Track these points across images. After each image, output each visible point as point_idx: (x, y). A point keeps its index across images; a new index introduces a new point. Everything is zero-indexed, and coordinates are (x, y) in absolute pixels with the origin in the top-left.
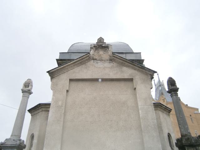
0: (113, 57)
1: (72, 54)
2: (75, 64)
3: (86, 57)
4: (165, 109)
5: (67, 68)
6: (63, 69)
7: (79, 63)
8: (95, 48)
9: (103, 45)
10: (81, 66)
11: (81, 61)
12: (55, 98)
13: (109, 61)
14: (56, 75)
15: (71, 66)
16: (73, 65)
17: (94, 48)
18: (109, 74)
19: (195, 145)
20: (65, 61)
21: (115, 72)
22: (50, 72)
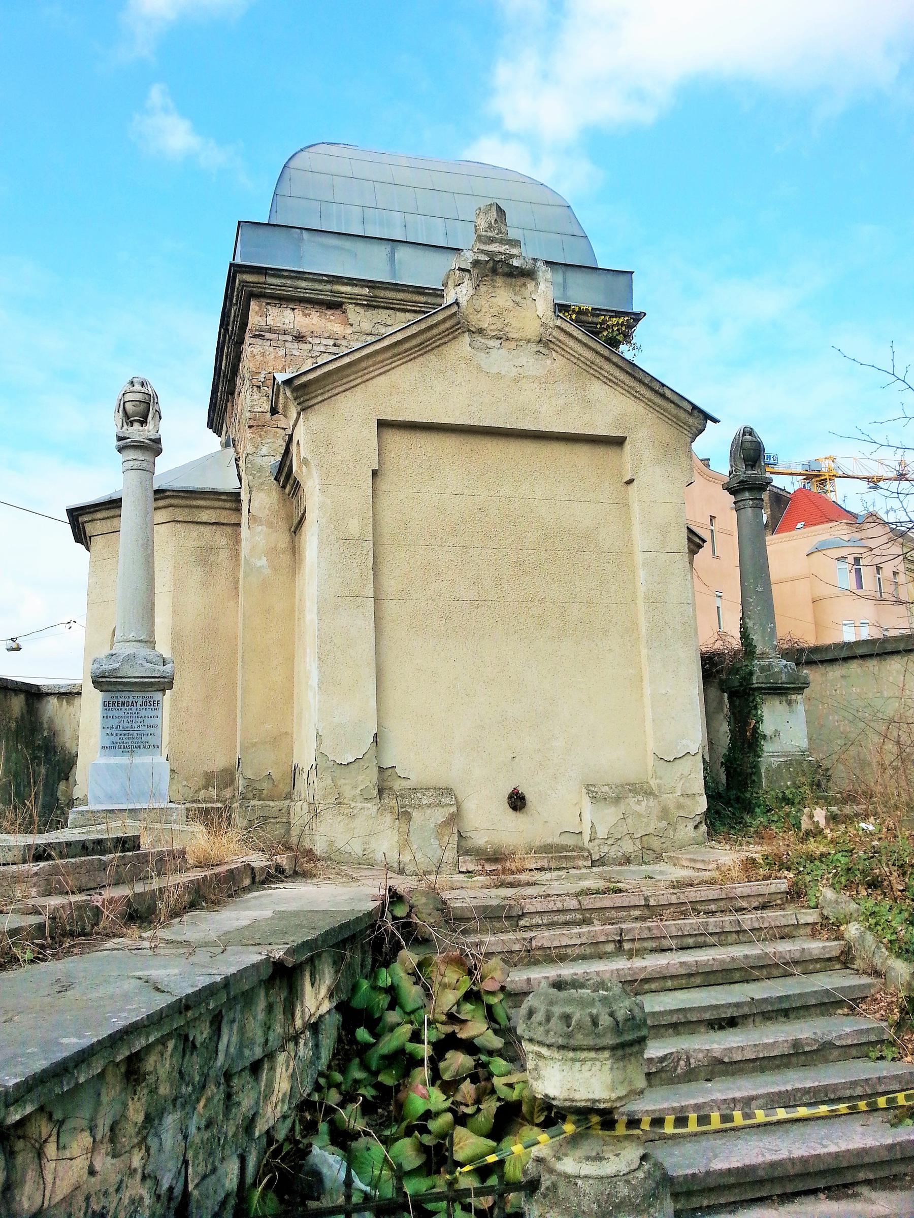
0: (556, 333)
1: (305, 234)
2: (396, 351)
5: (364, 365)
6: (349, 371)
8: (476, 271)
10: (421, 359)
12: (329, 501)
13: (534, 347)
14: (320, 398)
16: (389, 354)
17: (475, 272)
19: (788, 688)
20: (274, 276)
21: (561, 402)
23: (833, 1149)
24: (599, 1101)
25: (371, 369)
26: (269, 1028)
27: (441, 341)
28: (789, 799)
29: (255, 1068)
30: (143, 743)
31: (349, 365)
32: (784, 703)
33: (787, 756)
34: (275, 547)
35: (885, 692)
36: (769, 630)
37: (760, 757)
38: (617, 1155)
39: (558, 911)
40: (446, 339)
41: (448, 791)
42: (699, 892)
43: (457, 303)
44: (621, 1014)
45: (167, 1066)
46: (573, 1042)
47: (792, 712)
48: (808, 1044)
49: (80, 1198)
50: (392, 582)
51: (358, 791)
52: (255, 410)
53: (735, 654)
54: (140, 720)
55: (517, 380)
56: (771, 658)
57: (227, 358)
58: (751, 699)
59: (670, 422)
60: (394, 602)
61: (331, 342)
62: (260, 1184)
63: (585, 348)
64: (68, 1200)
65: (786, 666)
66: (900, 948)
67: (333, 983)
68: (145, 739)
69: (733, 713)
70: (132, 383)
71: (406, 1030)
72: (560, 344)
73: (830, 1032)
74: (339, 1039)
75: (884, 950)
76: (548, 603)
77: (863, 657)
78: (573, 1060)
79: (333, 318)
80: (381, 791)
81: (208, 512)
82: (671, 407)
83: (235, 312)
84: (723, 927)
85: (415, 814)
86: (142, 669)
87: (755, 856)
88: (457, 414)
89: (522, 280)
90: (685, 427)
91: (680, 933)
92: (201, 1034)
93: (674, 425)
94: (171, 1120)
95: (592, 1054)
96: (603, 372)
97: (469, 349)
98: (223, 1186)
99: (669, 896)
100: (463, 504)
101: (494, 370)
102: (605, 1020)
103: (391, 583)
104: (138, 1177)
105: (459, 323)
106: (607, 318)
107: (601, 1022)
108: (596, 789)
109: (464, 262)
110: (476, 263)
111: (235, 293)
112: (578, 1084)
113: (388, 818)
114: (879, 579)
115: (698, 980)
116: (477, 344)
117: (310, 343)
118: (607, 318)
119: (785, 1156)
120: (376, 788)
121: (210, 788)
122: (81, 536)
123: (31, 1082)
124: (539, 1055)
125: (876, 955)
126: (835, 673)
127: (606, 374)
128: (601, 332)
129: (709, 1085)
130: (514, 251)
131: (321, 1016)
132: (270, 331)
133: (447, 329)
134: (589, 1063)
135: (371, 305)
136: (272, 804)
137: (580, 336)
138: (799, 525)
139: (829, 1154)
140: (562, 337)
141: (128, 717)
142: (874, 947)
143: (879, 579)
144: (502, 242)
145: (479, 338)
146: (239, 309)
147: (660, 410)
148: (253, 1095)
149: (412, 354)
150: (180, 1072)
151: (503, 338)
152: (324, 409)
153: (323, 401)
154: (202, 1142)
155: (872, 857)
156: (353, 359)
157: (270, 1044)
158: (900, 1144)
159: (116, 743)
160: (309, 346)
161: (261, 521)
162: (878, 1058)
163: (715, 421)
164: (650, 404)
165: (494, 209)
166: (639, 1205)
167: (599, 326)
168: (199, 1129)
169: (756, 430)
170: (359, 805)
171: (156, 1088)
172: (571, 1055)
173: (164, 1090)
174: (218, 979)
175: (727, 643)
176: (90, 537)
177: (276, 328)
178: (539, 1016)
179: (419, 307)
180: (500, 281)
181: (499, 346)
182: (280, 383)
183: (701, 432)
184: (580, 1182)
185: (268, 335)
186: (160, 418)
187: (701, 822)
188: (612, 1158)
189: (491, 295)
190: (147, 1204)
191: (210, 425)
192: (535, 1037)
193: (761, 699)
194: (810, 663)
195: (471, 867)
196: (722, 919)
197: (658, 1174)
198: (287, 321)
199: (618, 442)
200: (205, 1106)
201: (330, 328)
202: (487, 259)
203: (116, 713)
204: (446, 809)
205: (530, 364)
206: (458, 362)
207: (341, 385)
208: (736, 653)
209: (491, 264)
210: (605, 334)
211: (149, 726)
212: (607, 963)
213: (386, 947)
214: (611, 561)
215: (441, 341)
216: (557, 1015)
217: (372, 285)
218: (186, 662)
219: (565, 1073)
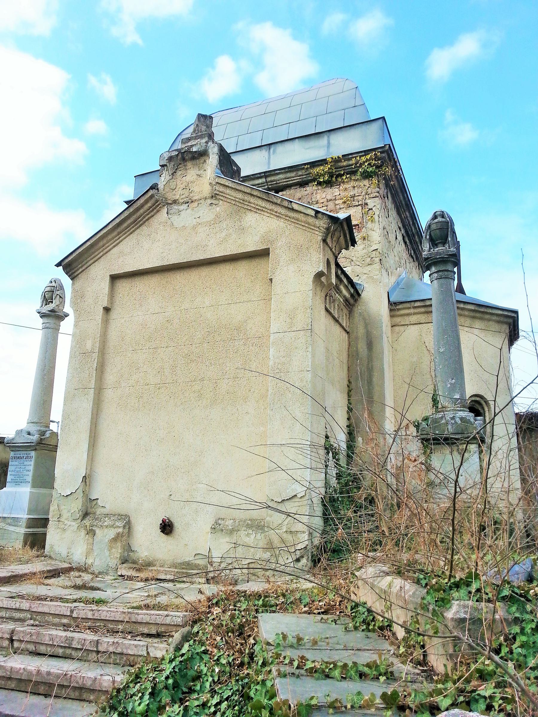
2: (119, 230)
3: (146, 202)
4: (478, 315)
5: (101, 244)
6: (93, 250)
7: (131, 223)
9: (194, 149)
11: (135, 217)
14: (81, 270)
15: (110, 237)
16: (115, 233)
17: (171, 166)
22: (63, 264)
25: (107, 245)
27: (149, 216)
31: (92, 246)
36: (449, 385)
39: (15, 609)
40: (152, 213)
42: (109, 613)
50: (111, 377)
54: (24, 467)
59: (304, 228)
63: (237, 192)
72: (222, 194)
76: (206, 381)
84: (83, 645)
85: (98, 531)
88: (155, 260)
90: (315, 229)
91: (51, 643)
93: (307, 229)
96: (252, 205)
100: (157, 319)
103: (110, 378)
105: (157, 201)
106: (358, 158)
109: (163, 161)
113: (83, 533)
115: (13, 685)
118: (358, 158)
127: (254, 206)
133: (151, 207)
140: (222, 189)
147: (295, 221)
149: (131, 229)
151: (189, 202)
152: (83, 276)
180: (189, 164)
199: (264, 254)
202: (177, 153)
204: (116, 529)
207: (91, 259)
209: (180, 156)
214: (254, 344)
215: (149, 216)
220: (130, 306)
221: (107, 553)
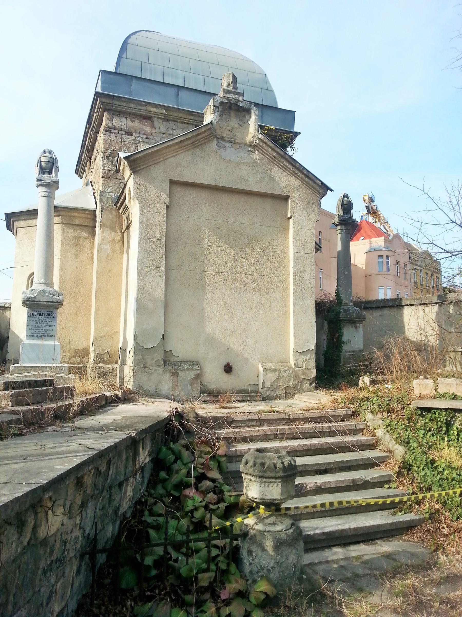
2: (180, 145)
5: (164, 151)
8: (222, 107)
9: (241, 105)
14: (142, 167)
16: (177, 147)
18: (247, 180)
19: (355, 321)
20: (117, 100)
21: (259, 176)
23: (367, 524)
24: (276, 500)
26: (126, 467)
28: (353, 372)
29: (120, 485)
30: (47, 334)
31: (157, 151)
32: (354, 327)
33: (353, 352)
34: (114, 240)
35: (399, 324)
36: (349, 292)
37: (341, 352)
38: (282, 523)
41: (196, 363)
43: (211, 123)
44: (286, 464)
45: (91, 481)
46: (266, 475)
47: (357, 331)
48: (358, 481)
49: (59, 534)
50: (174, 261)
51: (154, 362)
52: (105, 169)
53: (331, 302)
55: (239, 164)
56: (349, 306)
57: (89, 139)
58: (339, 324)
60: (175, 271)
61: (145, 137)
62: (123, 535)
64: (55, 534)
65: (356, 310)
66: (401, 440)
67: (151, 449)
68: (48, 332)
69: (329, 331)
70: (45, 152)
71: (184, 471)
73: (369, 476)
74: (152, 475)
75: (393, 441)
77: (390, 307)
78: (266, 482)
79: (146, 124)
80: (165, 362)
81: (79, 219)
82: (311, 182)
83: (96, 117)
85: (180, 373)
86: (48, 298)
87: (338, 397)
89: (244, 113)
92: (103, 468)
94: (91, 504)
95: (274, 480)
97: (216, 147)
98: (107, 535)
99: (299, 415)
101: (228, 158)
102: (279, 465)
104: (78, 528)
107: (278, 466)
108: (266, 365)
110: (222, 103)
111: (97, 107)
112: (266, 492)
113: (168, 375)
114: (397, 267)
116: (220, 145)
117: (134, 136)
118: (282, 134)
119: (347, 528)
120: (163, 360)
121: (77, 357)
122: (10, 227)
123: (51, 483)
124: (250, 480)
125: (390, 443)
126: (378, 313)
128: (278, 141)
129: (315, 498)
130: (241, 98)
131: (146, 464)
132: (114, 128)
134: (272, 484)
135: (166, 119)
136: (108, 366)
137: (269, 143)
138: (362, 238)
139: (366, 527)
140: (262, 144)
141: (40, 321)
142: (389, 440)
143: (397, 267)
144: (235, 93)
145: (222, 142)
146: (98, 115)
148: (119, 496)
149: (188, 147)
150: (95, 484)
151: (233, 142)
153: (143, 168)
154: (100, 515)
155: (390, 400)
156: (159, 148)
157: (127, 474)
158: (395, 523)
159: (34, 334)
160: (133, 138)
161: (107, 226)
162: (388, 488)
163: (332, 190)
164: (302, 180)
165: (231, 76)
166: (290, 543)
167: (277, 138)
168: (99, 509)
169: (349, 195)
170: (154, 368)
171: (86, 490)
172: (264, 480)
173: (89, 491)
174: (113, 444)
175: (327, 297)
176: (17, 228)
177: (117, 127)
178: (251, 463)
179: (190, 121)
180: (233, 113)
181: (231, 146)
182: (122, 158)
183: (324, 195)
184: (266, 534)
185: (113, 131)
186: (58, 170)
187: (313, 382)
188: (280, 524)
189: (228, 120)
190: (80, 540)
191: (77, 172)
192: (249, 472)
193: (343, 325)
194: (366, 308)
195: (206, 399)
196: (323, 426)
197: (298, 531)
198: (123, 124)
200: (102, 500)
201: (144, 129)
202: (227, 101)
203: (34, 319)
204: (195, 371)
205: (246, 156)
206: (210, 153)
208: (331, 301)
209: (229, 105)
210: (280, 142)
211: (50, 326)
212: (271, 444)
213: (176, 433)
216: (259, 463)
217: (167, 108)
218: (66, 294)
219: (261, 488)
220: (186, 208)
221: (190, 388)
